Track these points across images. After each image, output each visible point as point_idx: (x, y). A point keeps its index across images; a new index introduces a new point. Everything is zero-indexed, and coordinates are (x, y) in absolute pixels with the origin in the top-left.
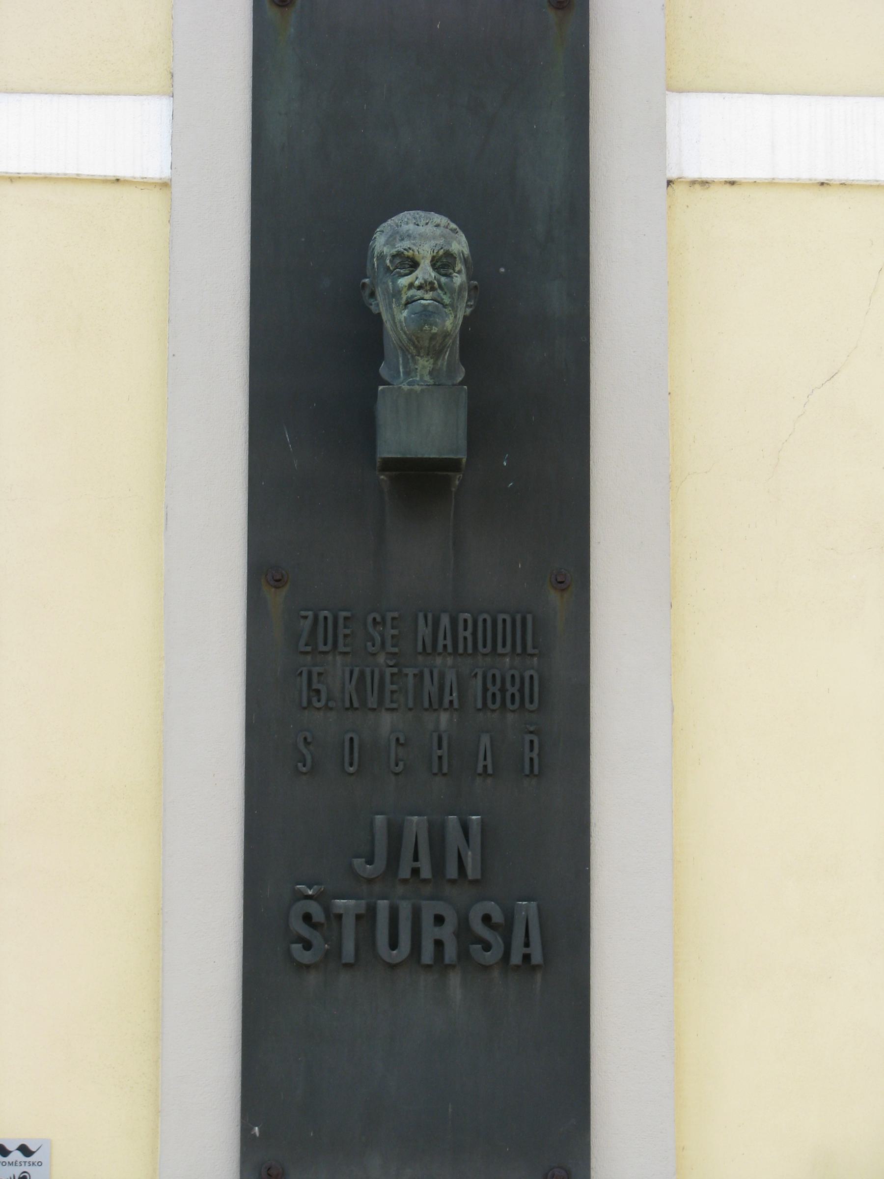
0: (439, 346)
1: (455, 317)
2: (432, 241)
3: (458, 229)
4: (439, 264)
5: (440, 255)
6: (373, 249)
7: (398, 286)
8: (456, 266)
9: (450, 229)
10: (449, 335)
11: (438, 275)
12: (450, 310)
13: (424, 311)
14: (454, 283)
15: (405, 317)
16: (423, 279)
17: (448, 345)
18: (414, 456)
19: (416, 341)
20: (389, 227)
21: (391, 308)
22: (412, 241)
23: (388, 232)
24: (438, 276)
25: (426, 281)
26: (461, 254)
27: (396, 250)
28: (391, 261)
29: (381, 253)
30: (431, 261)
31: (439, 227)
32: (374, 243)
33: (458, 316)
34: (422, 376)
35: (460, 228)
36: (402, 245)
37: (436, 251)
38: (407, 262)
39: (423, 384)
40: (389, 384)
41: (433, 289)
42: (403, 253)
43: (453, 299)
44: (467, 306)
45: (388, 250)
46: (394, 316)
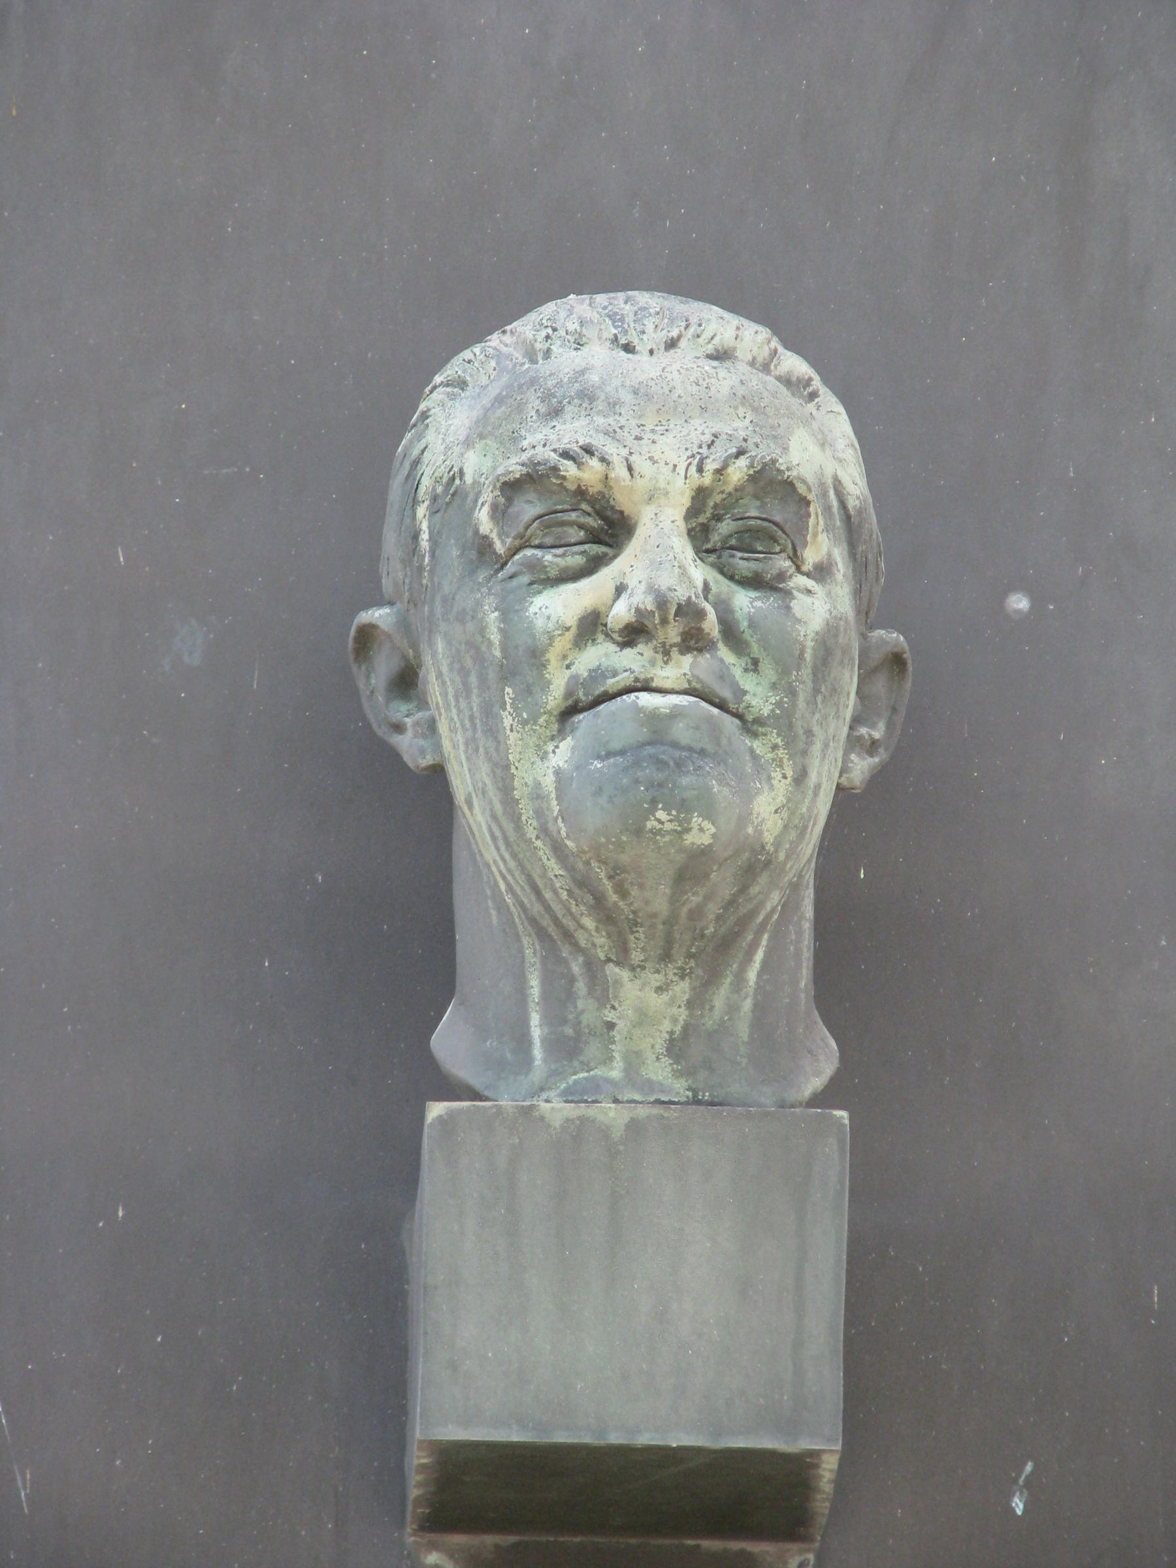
0: (719, 918)
1: (800, 778)
2: (696, 422)
3: (817, 383)
4: (726, 527)
5: (729, 488)
6: (416, 463)
7: (531, 627)
8: (805, 545)
9: (779, 378)
10: (768, 863)
11: (720, 577)
12: (775, 747)
13: (649, 744)
14: (799, 621)
15: (558, 772)
16: (652, 589)
17: (761, 918)
18: (588, 1439)
19: (608, 886)
20: (493, 363)
21: (493, 731)
22: (599, 420)
23: (484, 387)
24: (722, 586)
25: (662, 603)
26: (832, 493)
27: (525, 457)
28: (499, 514)
29: (453, 479)
30: (692, 512)
31: (728, 364)
32: (420, 436)
33: (813, 778)
34: (633, 1062)
35: (825, 381)
36: (552, 437)
37: (716, 466)
38: (573, 516)
39: (637, 1097)
40: (476, 1096)
41: (694, 642)
42: (555, 469)
43: (792, 693)
44: (854, 743)
45: (487, 463)
46: (507, 767)
